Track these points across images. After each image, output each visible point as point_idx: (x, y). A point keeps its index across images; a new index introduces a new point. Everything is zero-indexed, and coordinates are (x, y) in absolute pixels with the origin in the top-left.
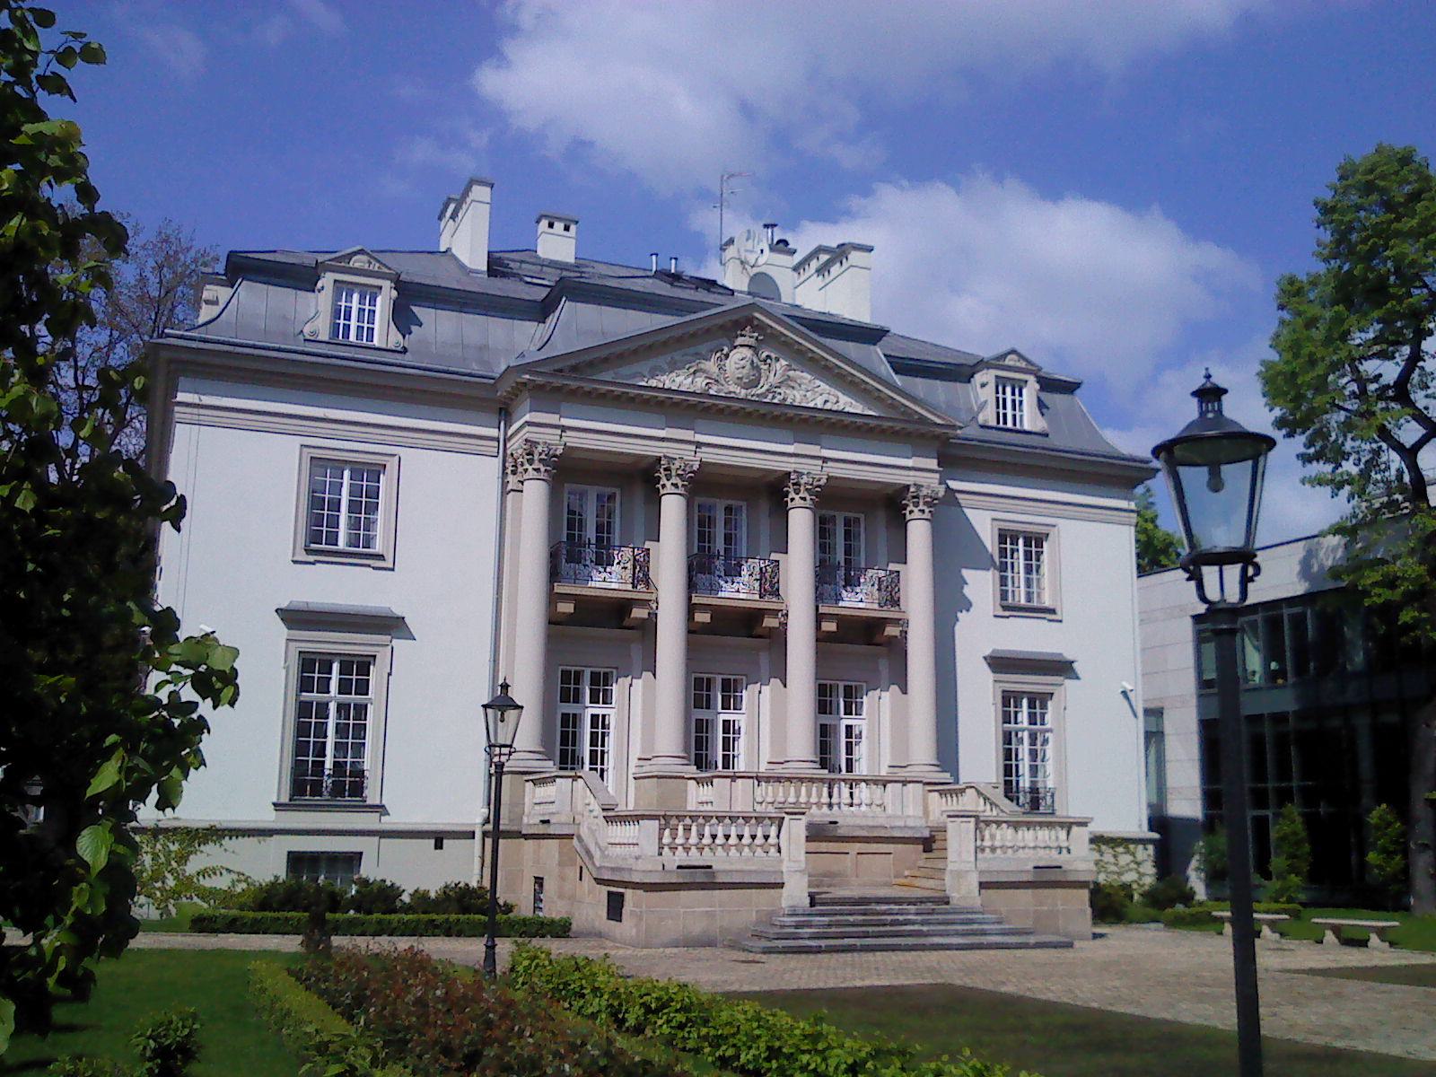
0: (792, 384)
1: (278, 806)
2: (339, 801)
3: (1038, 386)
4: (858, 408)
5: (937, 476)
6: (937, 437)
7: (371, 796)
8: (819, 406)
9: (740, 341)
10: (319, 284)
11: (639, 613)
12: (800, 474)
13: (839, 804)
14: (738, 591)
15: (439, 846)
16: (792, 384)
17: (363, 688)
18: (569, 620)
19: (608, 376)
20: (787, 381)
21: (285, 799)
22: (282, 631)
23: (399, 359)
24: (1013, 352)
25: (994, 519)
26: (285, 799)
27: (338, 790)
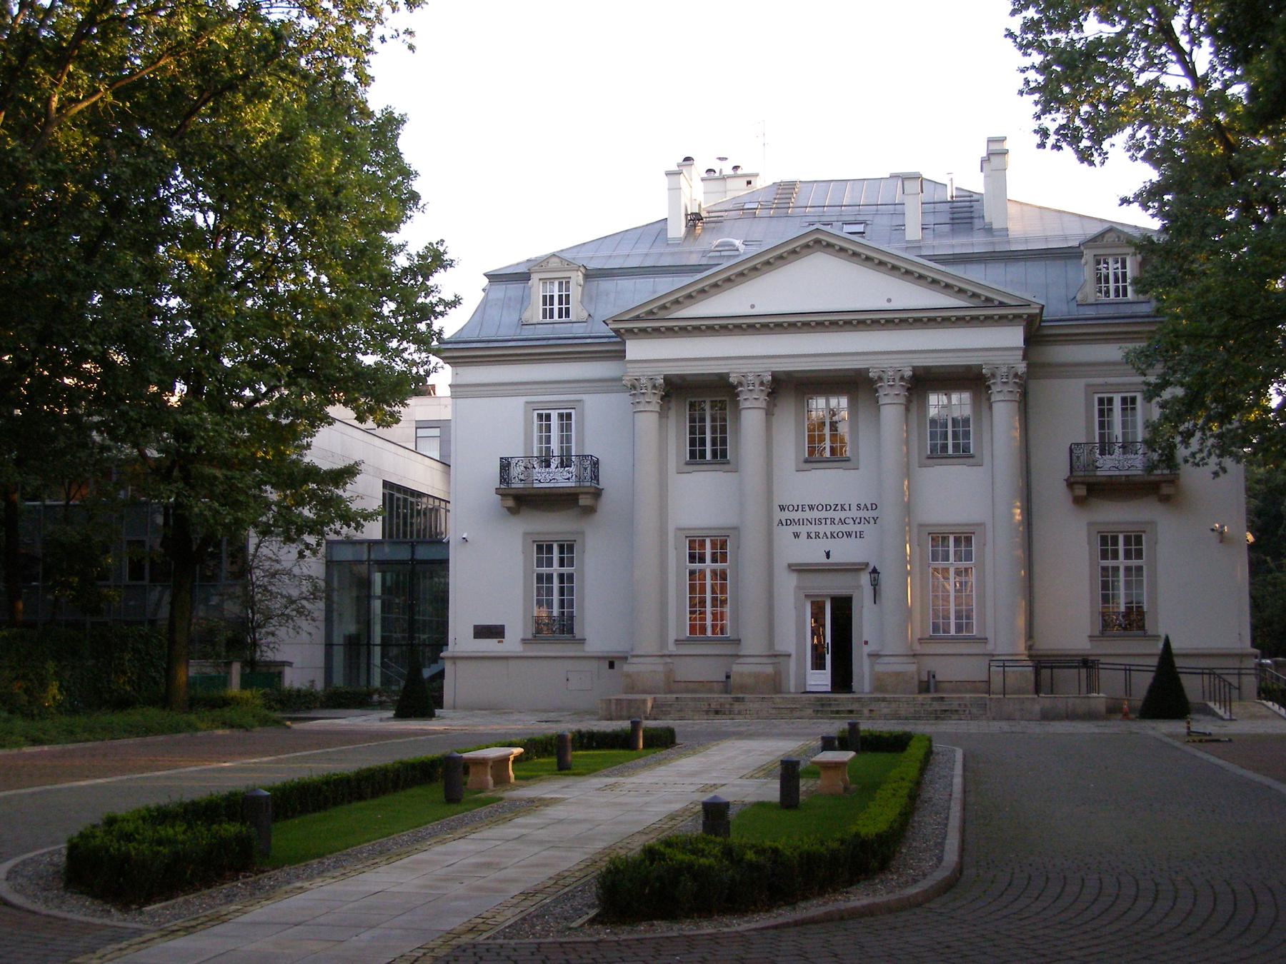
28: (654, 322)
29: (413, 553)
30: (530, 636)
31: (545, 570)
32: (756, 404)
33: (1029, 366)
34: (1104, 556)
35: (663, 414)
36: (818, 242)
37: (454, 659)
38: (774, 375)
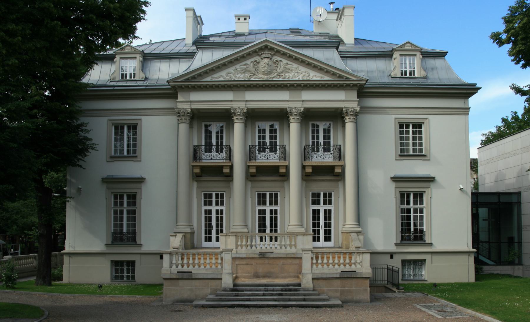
0: (287, 70)
1: (396, 244)
2: (404, 242)
3: (421, 56)
4: (326, 78)
5: (357, 103)
6: (354, 85)
7: (427, 240)
8: (301, 79)
9: (263, 56)
10: (115, 60)
11: (283, 170)
12: (292, 109)
13: (255, 245)
14: (211, 159)
15: (392, 257)
16: (287, 70)
17: (421, 203)
18: (253, 175)
19: (209, 79)
20: (286, 70)
21: (399, 242)
22: (393, 185)
23: (145, 83)
24: (408, 42)
25: (396, 118)
26: (399, 242)
27: (416, 238)
28: (193, 82)
29: (477, 199)
30: (110, 243)
31: (118, 208)
32: (185, 121)
33: (361, 108)
34: (402, 203)
35: (191, 126)
36: (266, 47)
37: (70, 254)
38: (248, 109)
